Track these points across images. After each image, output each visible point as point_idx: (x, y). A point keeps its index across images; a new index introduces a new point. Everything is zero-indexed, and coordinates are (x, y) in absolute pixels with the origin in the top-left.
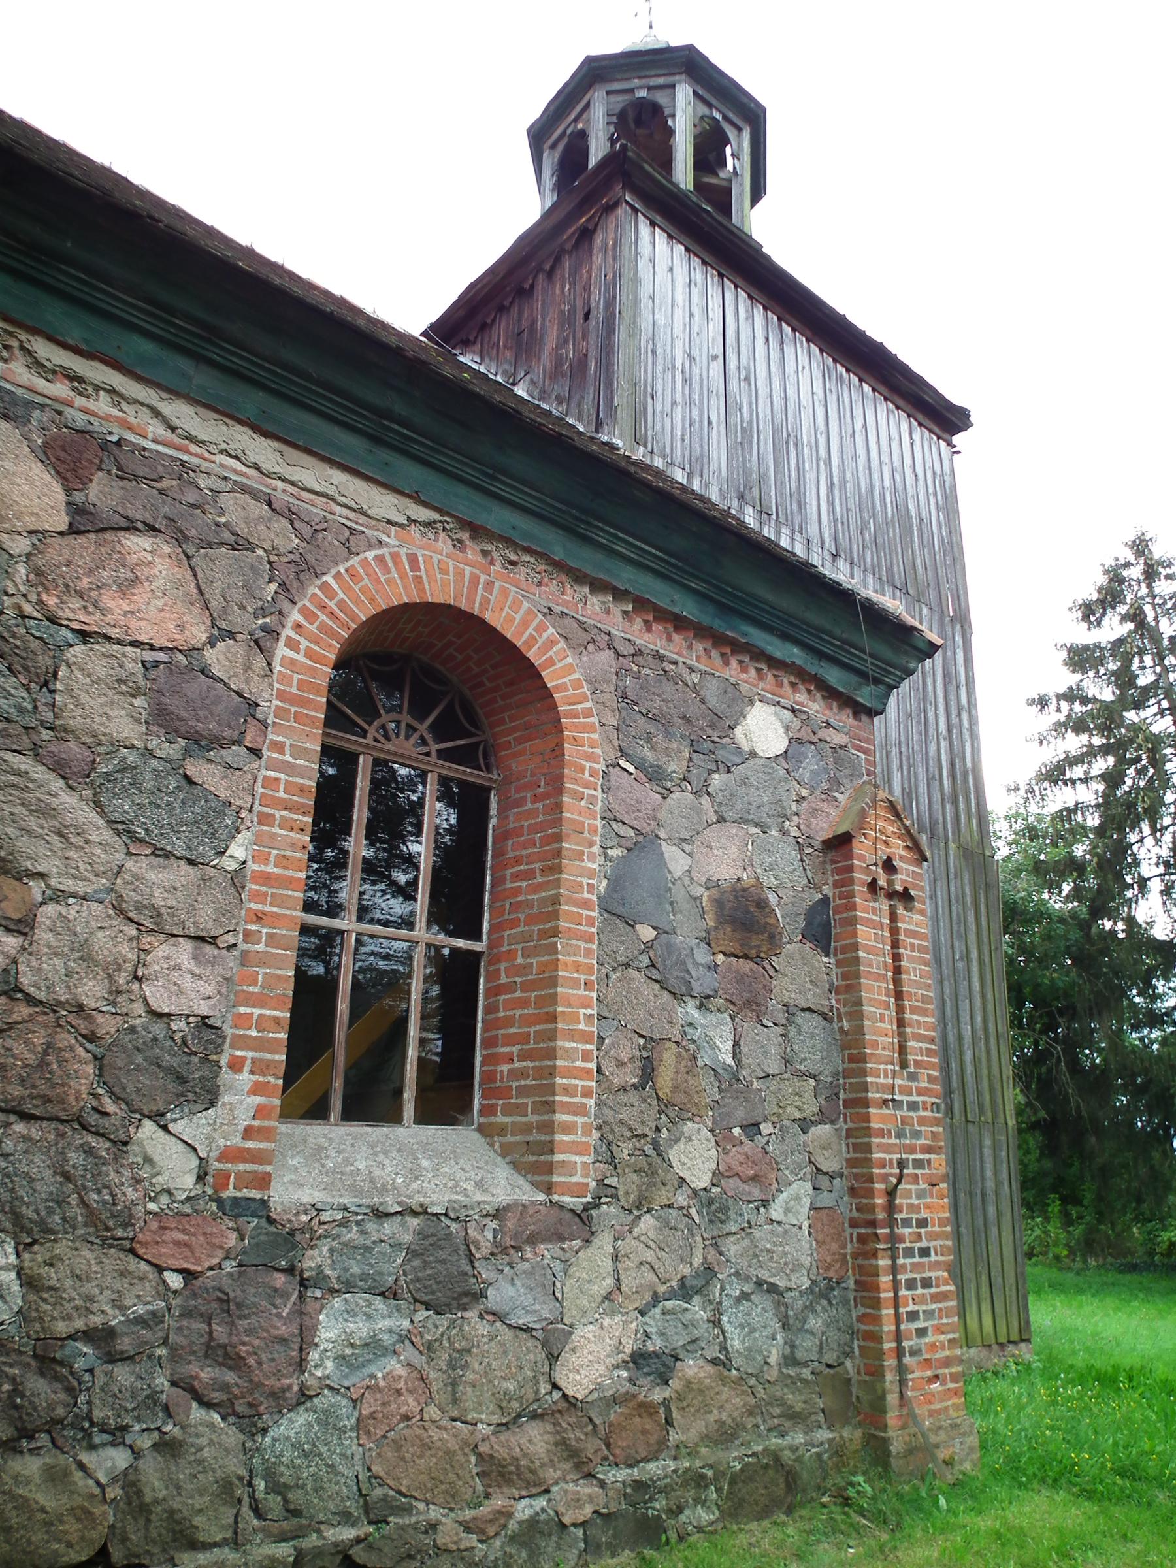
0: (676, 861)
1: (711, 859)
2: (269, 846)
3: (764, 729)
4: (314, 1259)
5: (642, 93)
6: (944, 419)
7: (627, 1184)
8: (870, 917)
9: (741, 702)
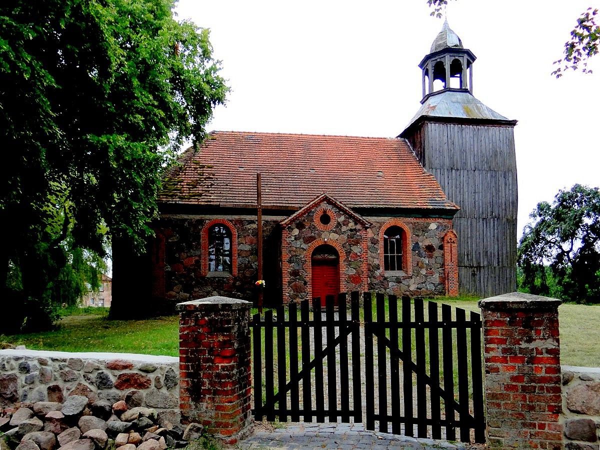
0: (420, 244)
1: (424, 242)
2: (381, 251)
3: (433, 226)
4: (388, 280)
5: (439, 60)
6: (513, 123)
7: (416, 274)
8: (447, 247)
9: (429, 224)
